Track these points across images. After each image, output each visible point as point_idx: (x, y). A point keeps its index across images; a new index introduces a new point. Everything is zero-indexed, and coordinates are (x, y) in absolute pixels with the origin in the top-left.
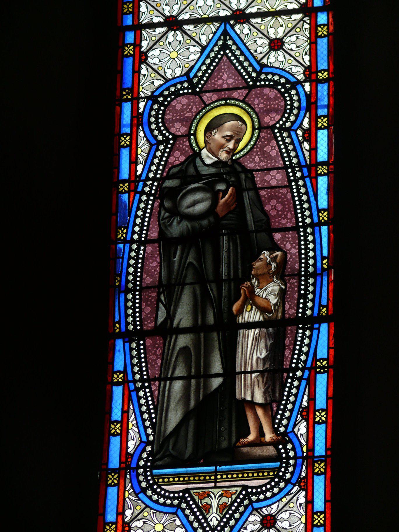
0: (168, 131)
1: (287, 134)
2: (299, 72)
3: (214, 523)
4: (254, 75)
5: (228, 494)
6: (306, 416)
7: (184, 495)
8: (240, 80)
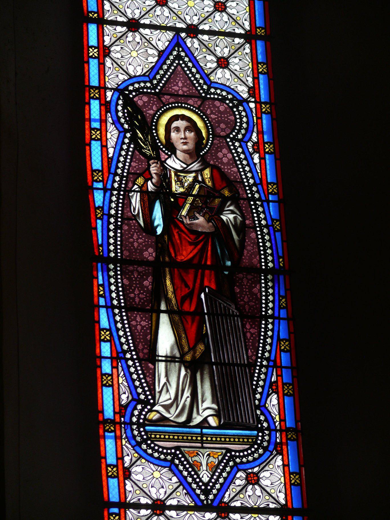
2: (243, 91)
6: (275, 389)
7: (176, 452)
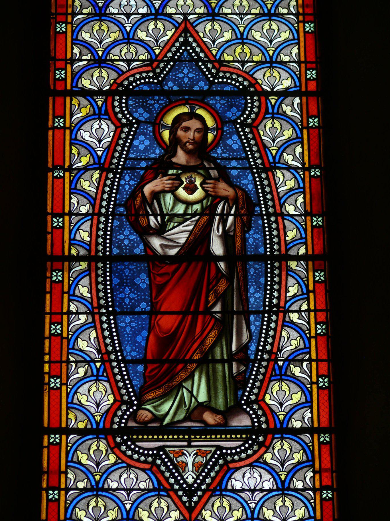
0: (131, 115)
1: (249, 129)
3: (190, 480)
4: (213, 71)
5: (204, 454)
8: (201, 75)
